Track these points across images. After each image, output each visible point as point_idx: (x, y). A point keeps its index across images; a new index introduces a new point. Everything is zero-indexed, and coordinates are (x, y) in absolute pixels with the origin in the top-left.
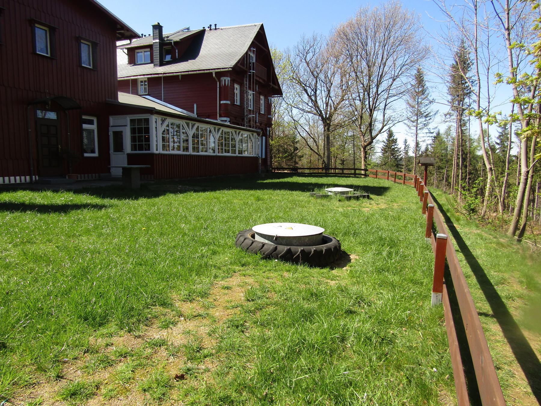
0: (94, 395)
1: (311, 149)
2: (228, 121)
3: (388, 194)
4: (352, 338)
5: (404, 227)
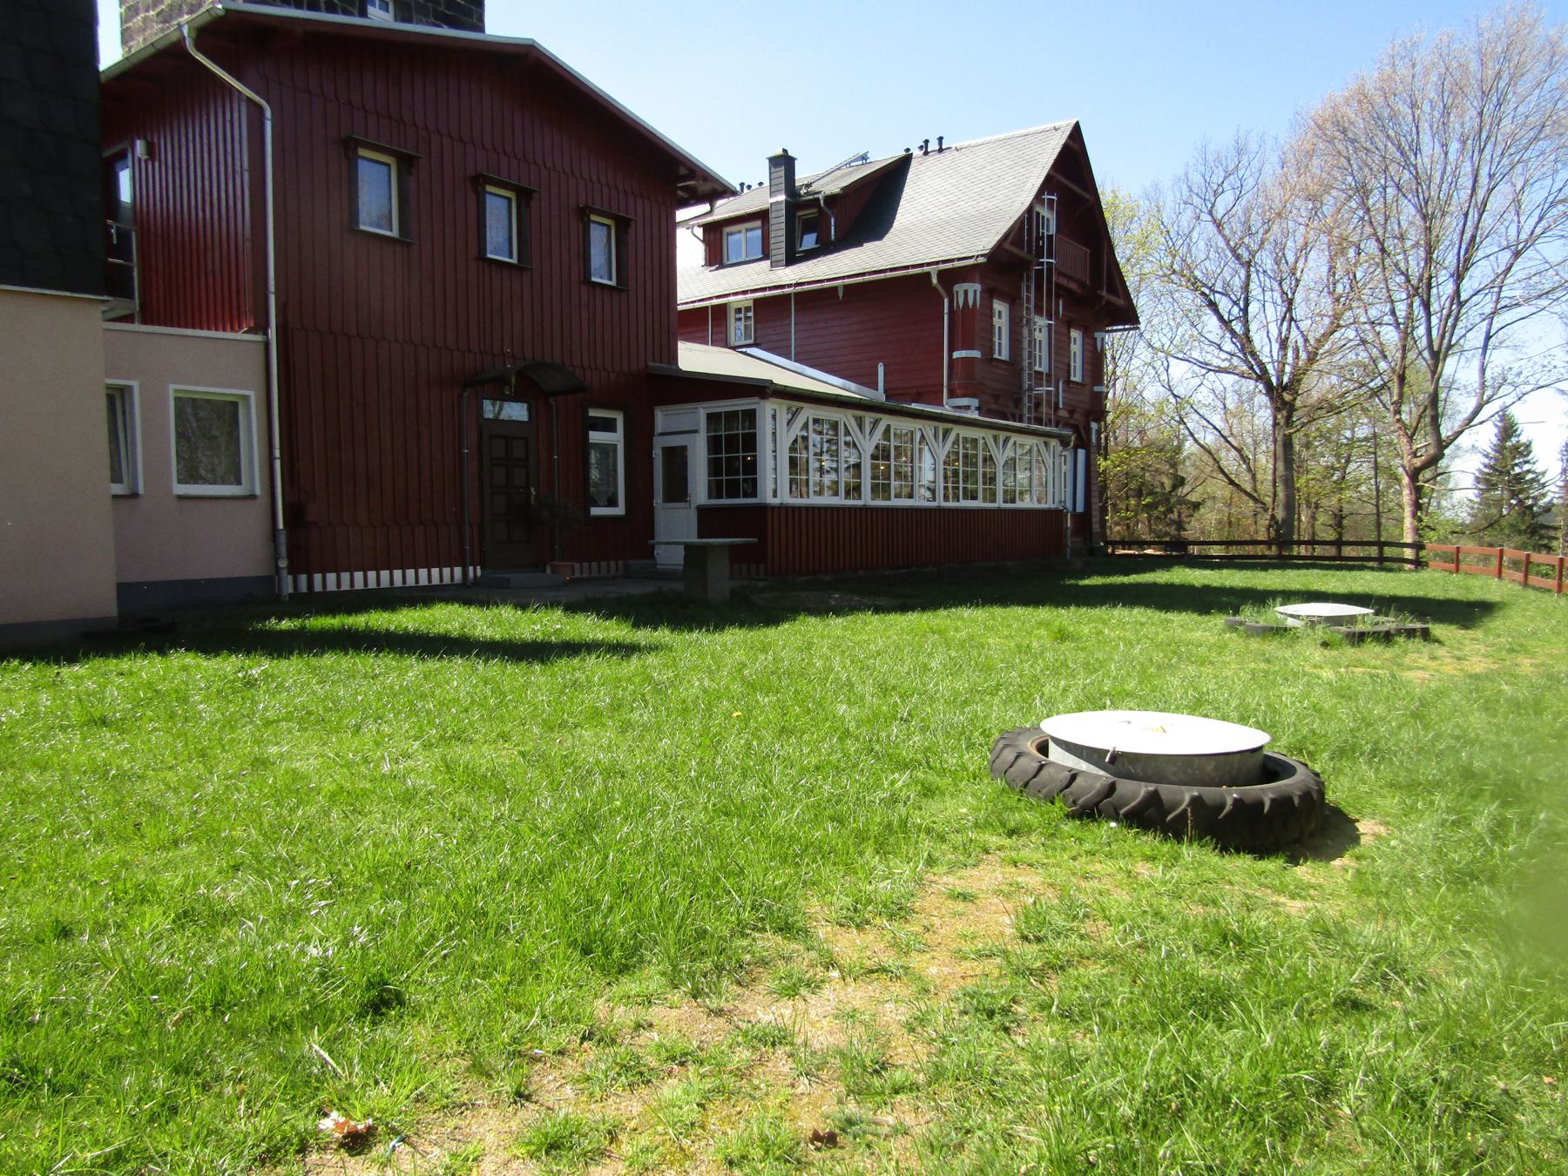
1: (1232, 482)
2: (973, 408)
3: (1496, 623)
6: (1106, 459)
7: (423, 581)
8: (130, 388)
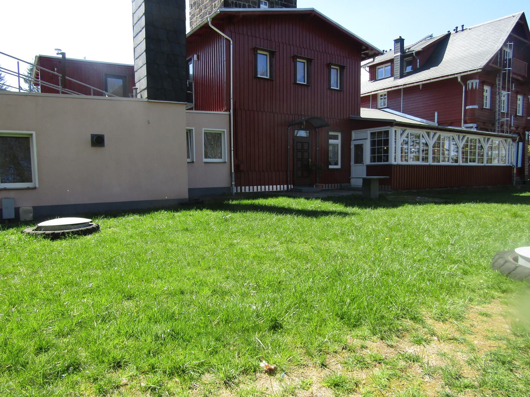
2: (474, 127)
7: (275, 189)
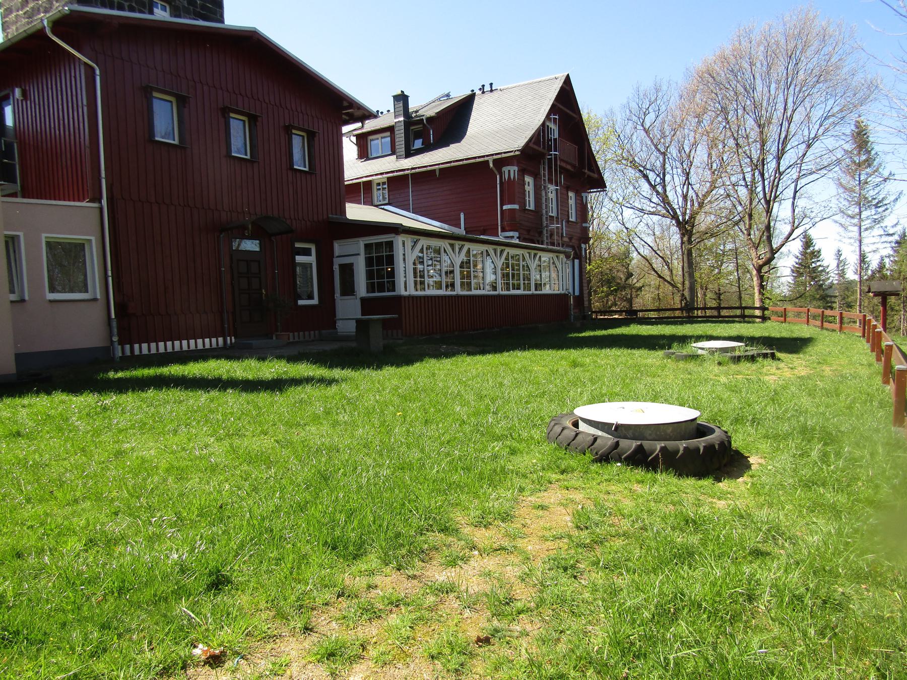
0: (359, 658)
1: (660, 276)
2: (515, 237)
3: (810, 349)
4: (767, 597)
5: (847, 408)
6: (589, 265)
7: (200, 346)
8: (18, 236)
